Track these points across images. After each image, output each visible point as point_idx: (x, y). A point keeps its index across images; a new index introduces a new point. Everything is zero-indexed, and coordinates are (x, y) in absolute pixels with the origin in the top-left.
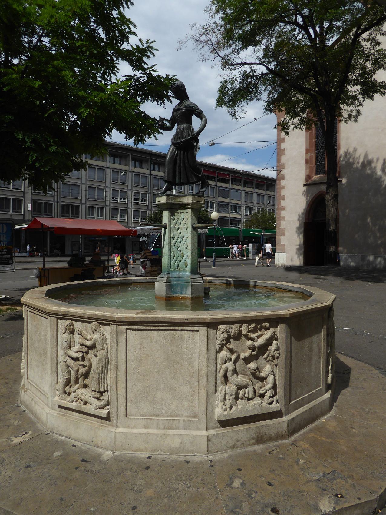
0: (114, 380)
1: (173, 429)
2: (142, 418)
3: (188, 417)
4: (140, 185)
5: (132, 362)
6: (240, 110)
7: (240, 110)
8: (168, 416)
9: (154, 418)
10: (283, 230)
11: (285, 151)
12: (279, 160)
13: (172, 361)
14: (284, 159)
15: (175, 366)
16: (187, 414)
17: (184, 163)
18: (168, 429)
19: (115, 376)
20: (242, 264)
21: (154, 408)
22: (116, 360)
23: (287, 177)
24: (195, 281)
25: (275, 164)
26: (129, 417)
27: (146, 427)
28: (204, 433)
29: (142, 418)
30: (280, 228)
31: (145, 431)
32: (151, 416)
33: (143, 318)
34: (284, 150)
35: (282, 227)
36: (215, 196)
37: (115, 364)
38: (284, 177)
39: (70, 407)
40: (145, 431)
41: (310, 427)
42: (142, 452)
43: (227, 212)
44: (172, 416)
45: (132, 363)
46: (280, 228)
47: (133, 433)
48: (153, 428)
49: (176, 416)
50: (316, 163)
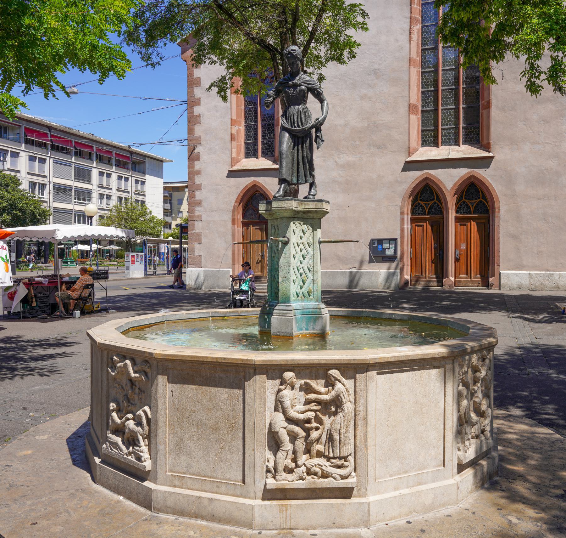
0: (363, 438)
1: (423, 484)
2: (391, 478)
3: (435, 466)
4: (73, 166)
5: (382, 412)
6: (155, 53)
7: (155, 53)
8: (416, 471)
9: (403, 476)
10: (199, 235)
11: (201, 118)
12: (191, 131)
13: (420, 404)
14: (198, 130)
15: (423, 410)
16: (434, 464)
17: (303, 157)
18: (418, 485)
19: (364, 433)
20: (123, 286)
21: (403, 464)
22: (365, 413)
23: (204, 157)
24: (286, 313)
25: (186, 136)
26: (379, 481)
27: (396, 489)
28: (371, 498)
29: (391, 478)
30: (194, 231)
31: (397, 493)
32: (400, 474)
33: (397, 357)
34: (199, 116)
35: (196, 231)
36: (46, 173)
37: (364, 418)
38: (200, 156)
39: (296, 487)
40: (397, 493)
41: (186, 520)
42: (397, 519)
43: (70, 202)
44: (420, 470)
45: (382, 414)
46: (194, 231)
47: (387, 498)
48: (403, 489)
49: (424, 469)
50: (245, 140)
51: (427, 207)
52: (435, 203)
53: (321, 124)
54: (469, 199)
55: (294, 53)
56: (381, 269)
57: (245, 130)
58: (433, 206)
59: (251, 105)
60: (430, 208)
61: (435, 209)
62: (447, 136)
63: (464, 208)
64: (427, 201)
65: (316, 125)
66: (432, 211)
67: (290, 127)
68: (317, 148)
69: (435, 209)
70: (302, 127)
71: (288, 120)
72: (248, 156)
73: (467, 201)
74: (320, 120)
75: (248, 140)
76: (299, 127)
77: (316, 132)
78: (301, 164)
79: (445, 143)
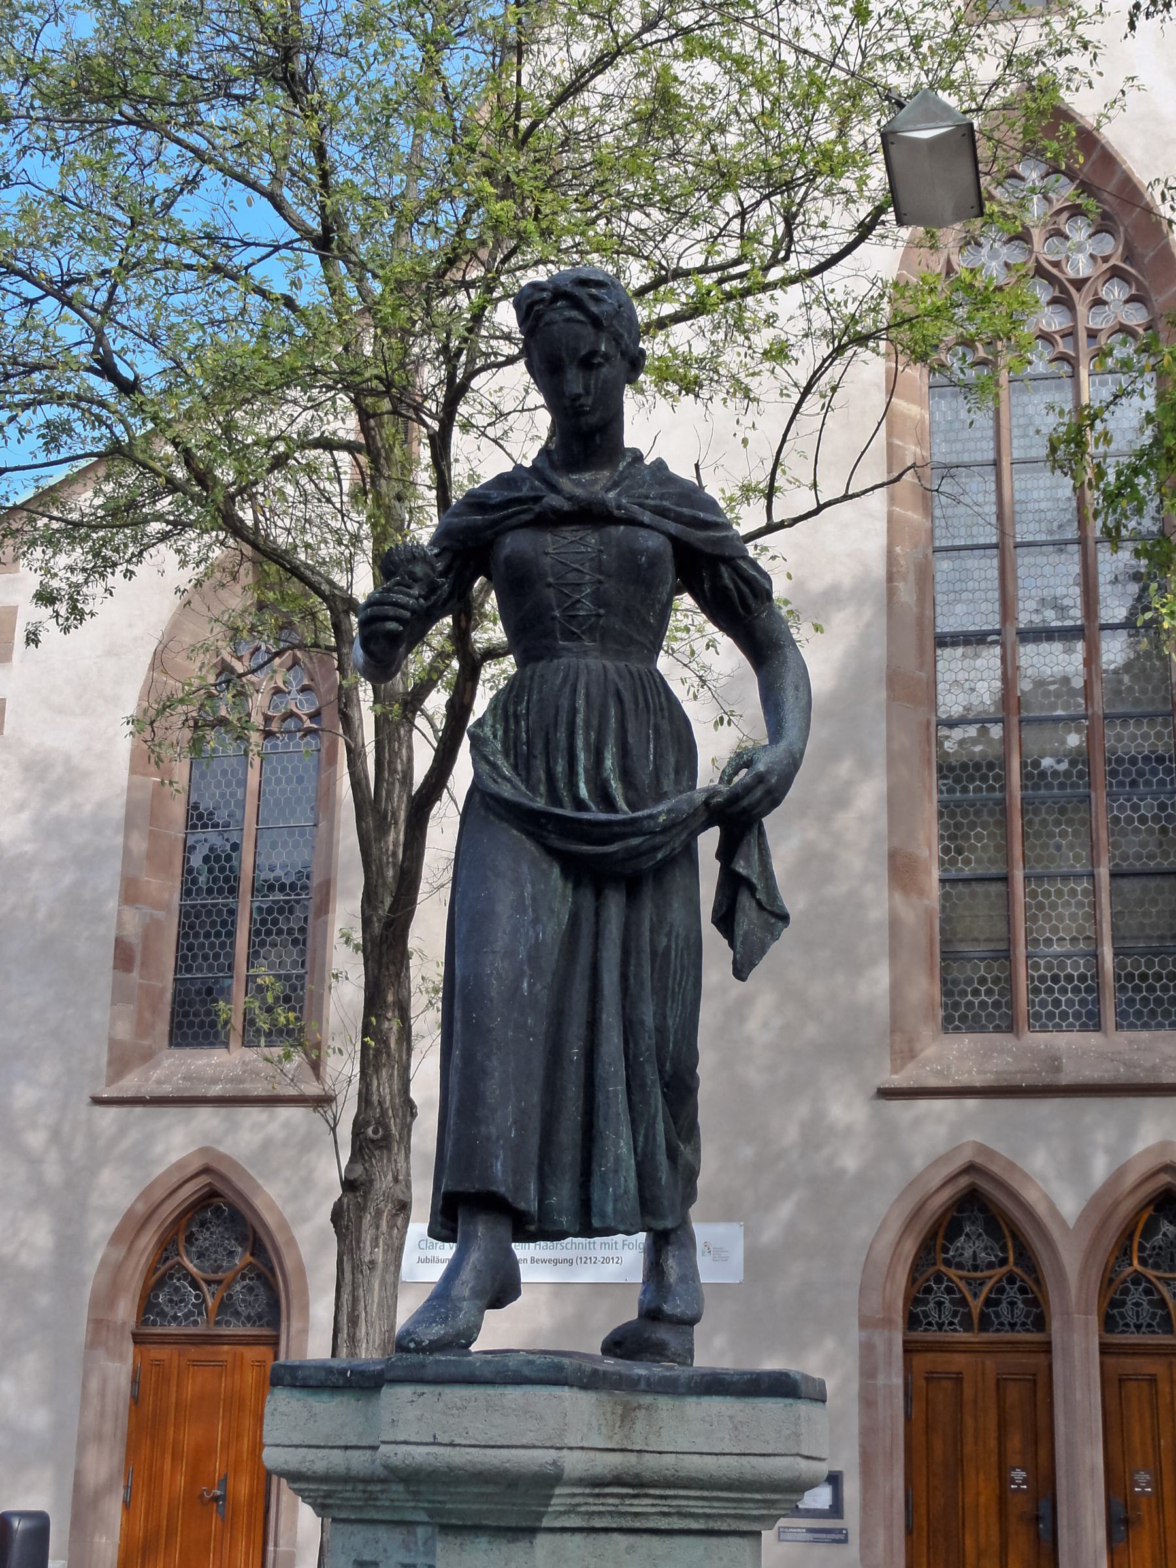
50: (177, 969)
51: (975, 1295)
52: (1011, 1279)
53: (774, 797)
54: (1156, 1266)
55: (597, 300)
56: (385, 1252)
57: (181, 925)
58: (1001, 1290)
59: (203, 906)
60: (988, 1302)
61: (1012, 1304)
62: (1050, 990)
63: (1137, 1304)
64: (975, 1268)
65: (735, 798)
66: (997, 1315)
67: (540, 804)
68: (741, 971)
69: (1012, 1304)
70: (633, 807)
71: (530, 755)
72: (184, 1036)
73: (1150, 1273)
74: (761, 767)
75: (189, 969)
76: (608, 803)
77: (726, 853)
78: (614, 1088)
79: (1042, 1021)
